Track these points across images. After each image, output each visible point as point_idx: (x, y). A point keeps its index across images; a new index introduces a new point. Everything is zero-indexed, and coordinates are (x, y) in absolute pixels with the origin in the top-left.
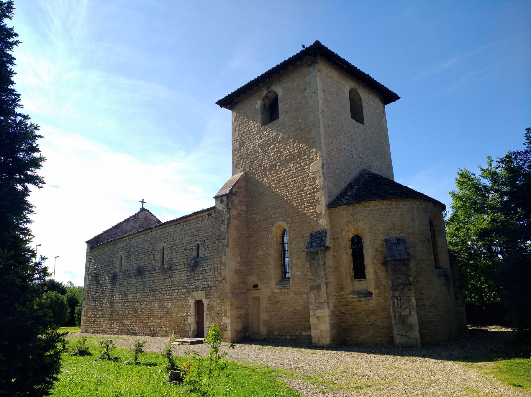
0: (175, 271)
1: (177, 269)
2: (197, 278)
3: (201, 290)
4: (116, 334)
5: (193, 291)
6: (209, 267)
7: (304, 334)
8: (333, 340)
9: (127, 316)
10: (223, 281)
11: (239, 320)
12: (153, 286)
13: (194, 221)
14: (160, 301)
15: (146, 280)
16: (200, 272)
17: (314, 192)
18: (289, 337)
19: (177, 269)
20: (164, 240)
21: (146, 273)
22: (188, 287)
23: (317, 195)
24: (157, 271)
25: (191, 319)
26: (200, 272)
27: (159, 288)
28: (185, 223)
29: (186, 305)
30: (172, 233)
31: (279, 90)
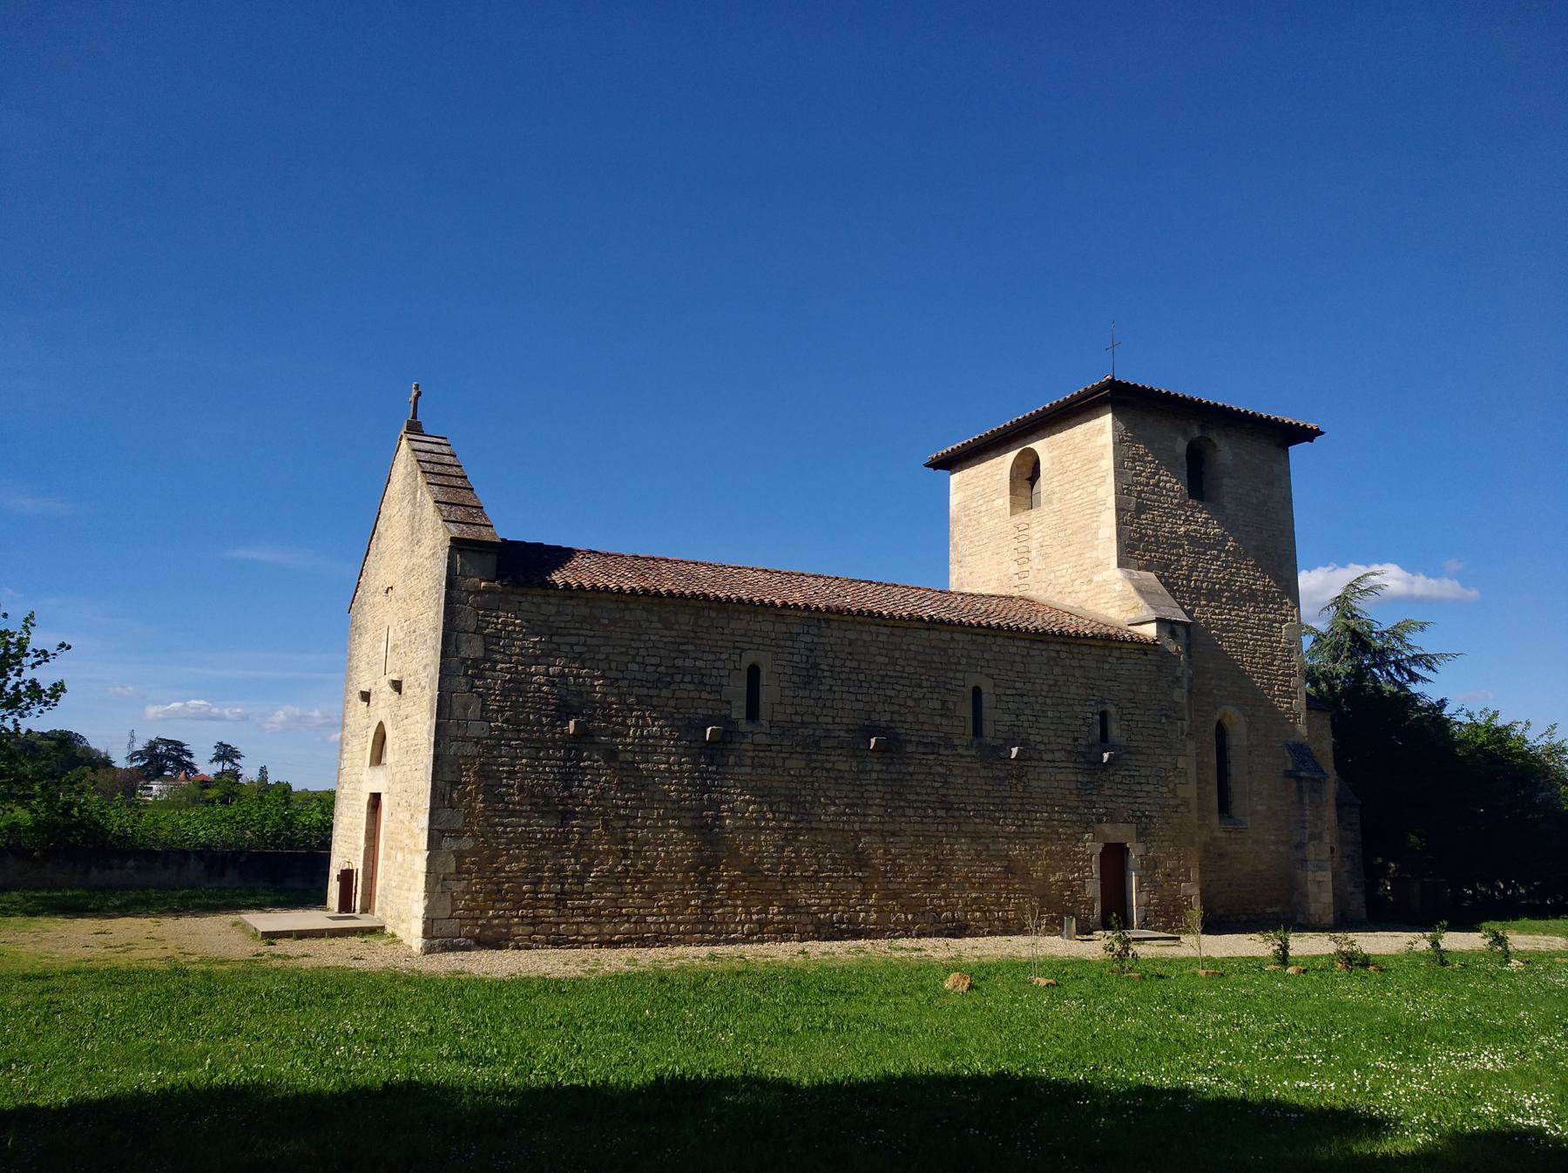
0: (1034, 763)
1: (1041, 759)
2: (1109, 792)
3: (1125, 821)
4: (745, 941)
5: (1100, 821)
6: (1143, 771)
7: (1269, 910)
8: (1336, 920)
9: (814, 878)
10: (1181, 809)
11: (45, 677)
12: (941, 792)
13: (1094, 651)
14: (974, 837)
15: (911, 769)
16: (1118, 779)
17: (1289, 675)
18: (1244, 918)
19: (1041, 759)
20: (991, 671)
21: (910, 748)
22: (1081, 810)
23: (1293, 682)
24: (961, 751)
25: (1093, 889)
26: (1118, 779)
27: (972, 799)
28: (1064, 648)
29: (1076, 853)
30: (1018, 658)
31: (1040, 446)
